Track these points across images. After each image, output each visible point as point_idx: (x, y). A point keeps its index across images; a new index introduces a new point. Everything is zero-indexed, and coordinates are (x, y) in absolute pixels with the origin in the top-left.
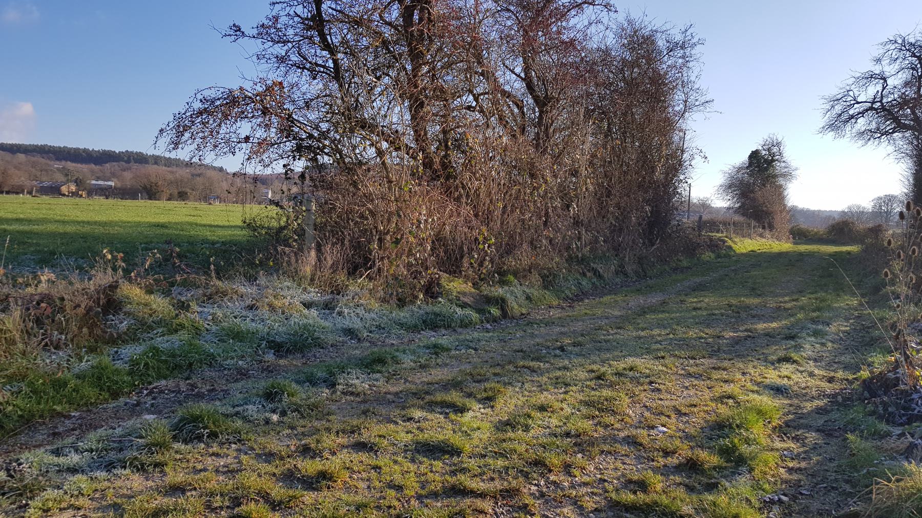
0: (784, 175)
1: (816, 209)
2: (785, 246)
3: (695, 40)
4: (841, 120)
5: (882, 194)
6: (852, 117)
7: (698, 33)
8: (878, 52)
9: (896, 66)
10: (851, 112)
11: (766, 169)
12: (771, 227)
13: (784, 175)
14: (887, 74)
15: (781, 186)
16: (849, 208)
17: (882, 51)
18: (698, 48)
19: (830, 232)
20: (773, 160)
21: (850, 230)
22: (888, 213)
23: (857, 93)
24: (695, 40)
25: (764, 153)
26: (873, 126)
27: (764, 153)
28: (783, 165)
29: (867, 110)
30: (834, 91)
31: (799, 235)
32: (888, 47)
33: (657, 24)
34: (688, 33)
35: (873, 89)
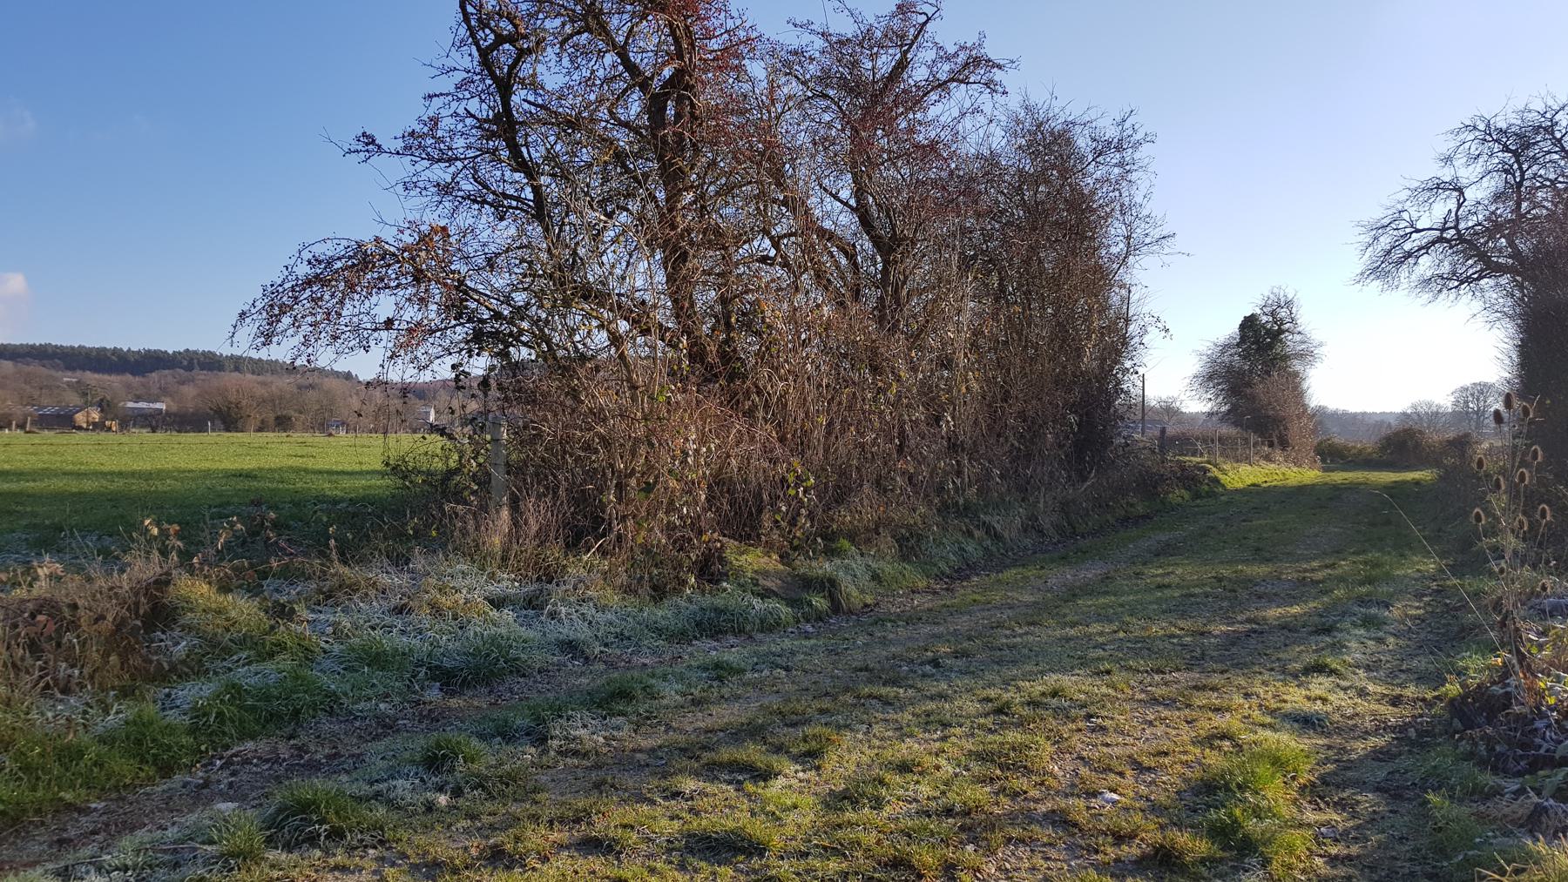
0: (1301, 356)
2: (1310, 474)
4: (1389, 262)
5: (1468, 382)
6: (1409, 255)
7: (1144, 123)
9: (1478, 168)
10: (1407, 246)
11: (1271, 346)
12: (1284, 444)
13: (1301, 356)
14: (1464, 182)
15: (1296, 374)
16: (1414, 406)
18: (1145, 149)
19: (1383, 449)
20: (1281, 331)
21: (1417, 445)
22: (1479, 413)
23: (1415, 215)
25: (1264, 319)
26: (1446, 268)
27: (1264, 319)
28: (1298, 338)
29: (1433, 243)
30: (1378, 213)
31: (1331, 455)
32: (1462, 137)
33: (1075, 112)
34: (1127, 125)
35: (1442, 207)
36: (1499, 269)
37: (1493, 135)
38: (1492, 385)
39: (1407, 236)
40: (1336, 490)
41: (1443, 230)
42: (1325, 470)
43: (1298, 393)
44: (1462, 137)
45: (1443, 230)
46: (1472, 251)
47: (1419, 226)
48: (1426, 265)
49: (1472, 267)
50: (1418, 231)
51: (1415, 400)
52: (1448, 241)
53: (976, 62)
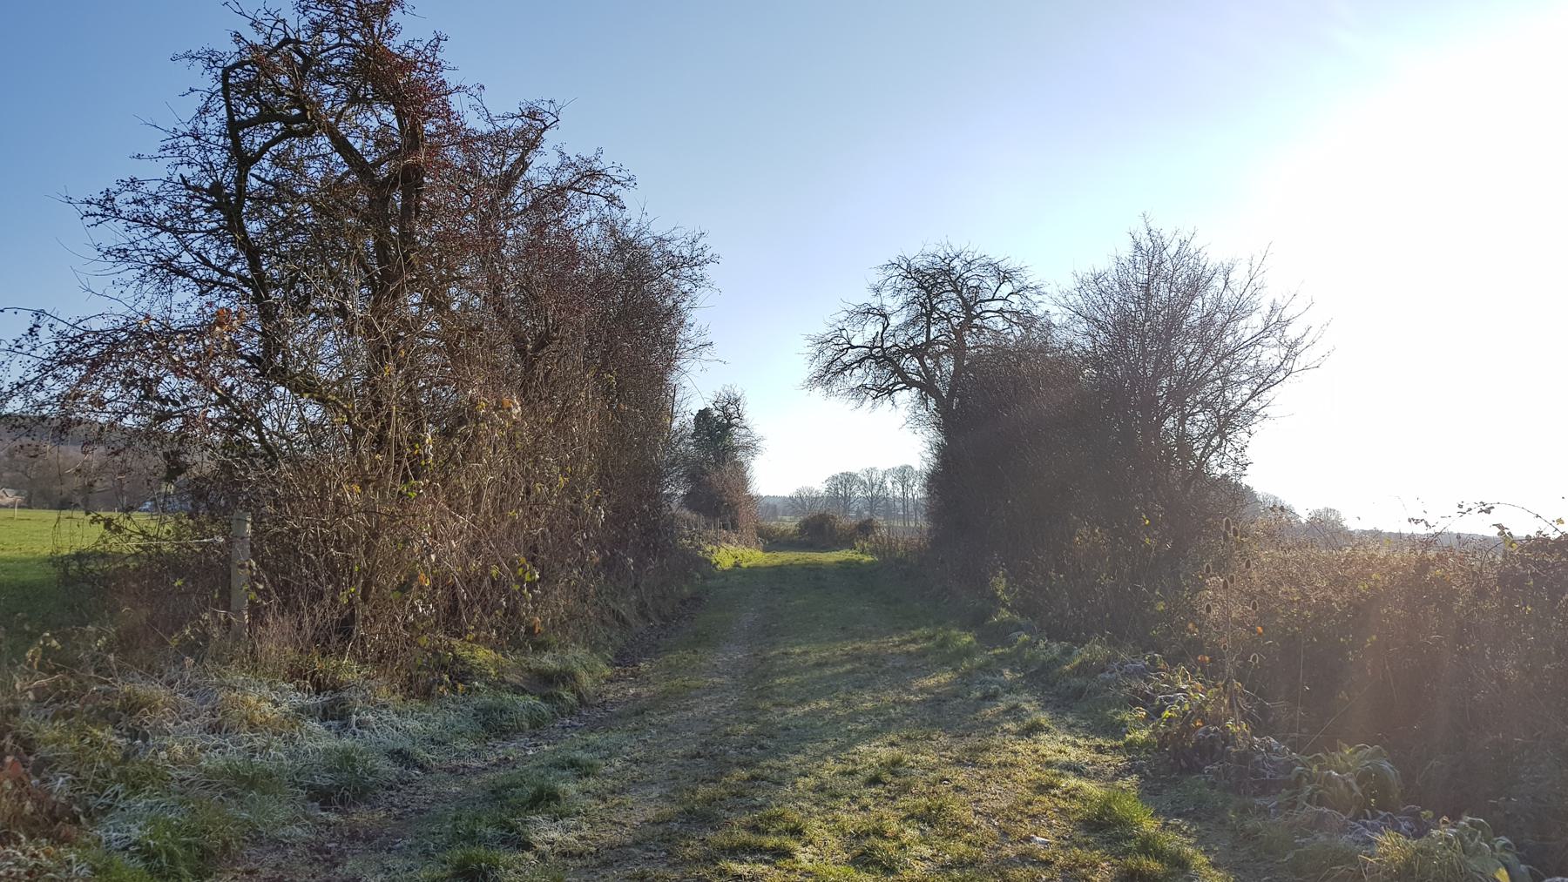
0: (746, 448)
1: (1393, 522)
2: (755, 557)
3: (707, 255)
4: (830, 373)
5: (837, 472)
6: (846, 367)
7: (712, 244)
8: (876, 278)
9: (901, 299)
10: (846, 359)
11: (721, 438)
12: (735, 526)
13: (746, 448)
14: (888, 310)
15: (742, 464)
16: (799, 491)
17: (882, 278)
18: (709, 269)
19: (801, 532)
20: (730, 425)
21: (832, 528)
22: (846, 498)
23: (851, 334)
24: (707, 255)
25: (716, 413)
26: (869, 381)
27: (716, 413)
28: (744, 432)
29: (863, 360)
30: (823, 330)
31: (772, 541)
32: (889, 272)
33: (658, 229)
34: (699, 245)
35: (873, 328)
36: (910, 384)
37: (912, 273)
38: (855, 476)
39: (844, 351)
40: (780, 570)
41: (871, 349)
42: (766, 550)
43: (744, 482)
44: (889, 272)
45: (871, 349)
46: (887, 366)
47: (854, 343)
48: (858, 376)
49: (885, 376)
50: (853, 347)
51: (799, 486)
52: (875, 358)
53: (594, 175)
